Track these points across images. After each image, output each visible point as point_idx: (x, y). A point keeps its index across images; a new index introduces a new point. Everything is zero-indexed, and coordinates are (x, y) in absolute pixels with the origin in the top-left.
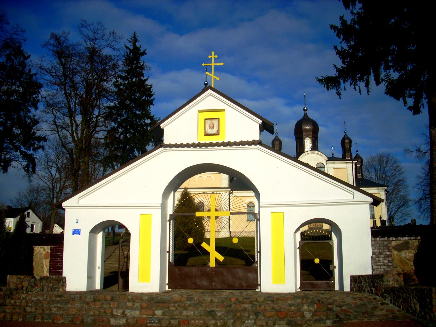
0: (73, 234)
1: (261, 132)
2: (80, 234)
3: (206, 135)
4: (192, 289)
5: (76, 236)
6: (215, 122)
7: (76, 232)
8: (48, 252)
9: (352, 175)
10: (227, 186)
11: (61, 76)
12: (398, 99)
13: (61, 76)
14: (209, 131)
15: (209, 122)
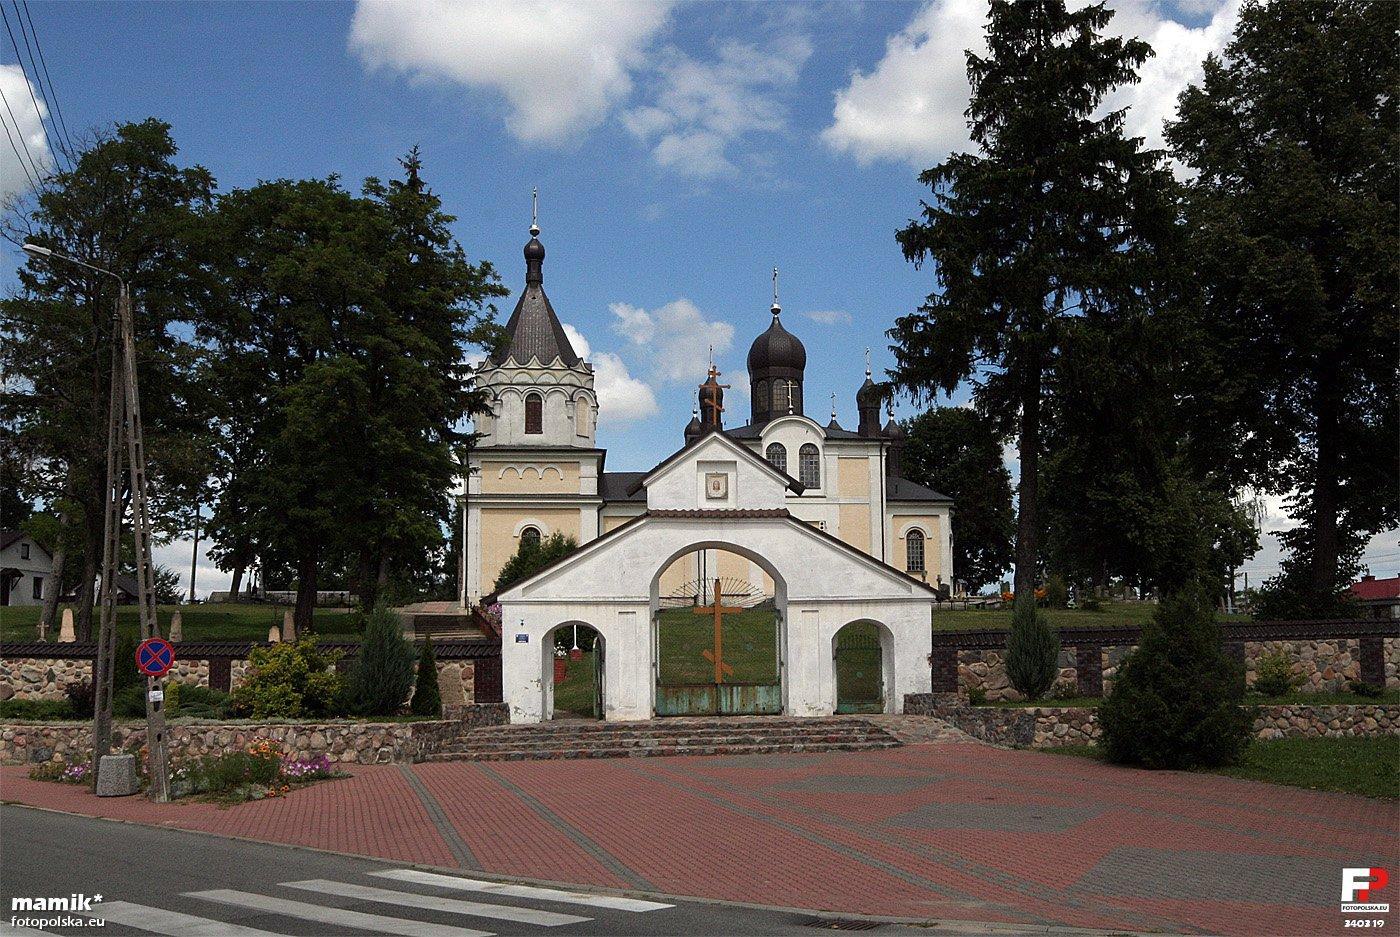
3: (710, 498)
6: (722, 481)
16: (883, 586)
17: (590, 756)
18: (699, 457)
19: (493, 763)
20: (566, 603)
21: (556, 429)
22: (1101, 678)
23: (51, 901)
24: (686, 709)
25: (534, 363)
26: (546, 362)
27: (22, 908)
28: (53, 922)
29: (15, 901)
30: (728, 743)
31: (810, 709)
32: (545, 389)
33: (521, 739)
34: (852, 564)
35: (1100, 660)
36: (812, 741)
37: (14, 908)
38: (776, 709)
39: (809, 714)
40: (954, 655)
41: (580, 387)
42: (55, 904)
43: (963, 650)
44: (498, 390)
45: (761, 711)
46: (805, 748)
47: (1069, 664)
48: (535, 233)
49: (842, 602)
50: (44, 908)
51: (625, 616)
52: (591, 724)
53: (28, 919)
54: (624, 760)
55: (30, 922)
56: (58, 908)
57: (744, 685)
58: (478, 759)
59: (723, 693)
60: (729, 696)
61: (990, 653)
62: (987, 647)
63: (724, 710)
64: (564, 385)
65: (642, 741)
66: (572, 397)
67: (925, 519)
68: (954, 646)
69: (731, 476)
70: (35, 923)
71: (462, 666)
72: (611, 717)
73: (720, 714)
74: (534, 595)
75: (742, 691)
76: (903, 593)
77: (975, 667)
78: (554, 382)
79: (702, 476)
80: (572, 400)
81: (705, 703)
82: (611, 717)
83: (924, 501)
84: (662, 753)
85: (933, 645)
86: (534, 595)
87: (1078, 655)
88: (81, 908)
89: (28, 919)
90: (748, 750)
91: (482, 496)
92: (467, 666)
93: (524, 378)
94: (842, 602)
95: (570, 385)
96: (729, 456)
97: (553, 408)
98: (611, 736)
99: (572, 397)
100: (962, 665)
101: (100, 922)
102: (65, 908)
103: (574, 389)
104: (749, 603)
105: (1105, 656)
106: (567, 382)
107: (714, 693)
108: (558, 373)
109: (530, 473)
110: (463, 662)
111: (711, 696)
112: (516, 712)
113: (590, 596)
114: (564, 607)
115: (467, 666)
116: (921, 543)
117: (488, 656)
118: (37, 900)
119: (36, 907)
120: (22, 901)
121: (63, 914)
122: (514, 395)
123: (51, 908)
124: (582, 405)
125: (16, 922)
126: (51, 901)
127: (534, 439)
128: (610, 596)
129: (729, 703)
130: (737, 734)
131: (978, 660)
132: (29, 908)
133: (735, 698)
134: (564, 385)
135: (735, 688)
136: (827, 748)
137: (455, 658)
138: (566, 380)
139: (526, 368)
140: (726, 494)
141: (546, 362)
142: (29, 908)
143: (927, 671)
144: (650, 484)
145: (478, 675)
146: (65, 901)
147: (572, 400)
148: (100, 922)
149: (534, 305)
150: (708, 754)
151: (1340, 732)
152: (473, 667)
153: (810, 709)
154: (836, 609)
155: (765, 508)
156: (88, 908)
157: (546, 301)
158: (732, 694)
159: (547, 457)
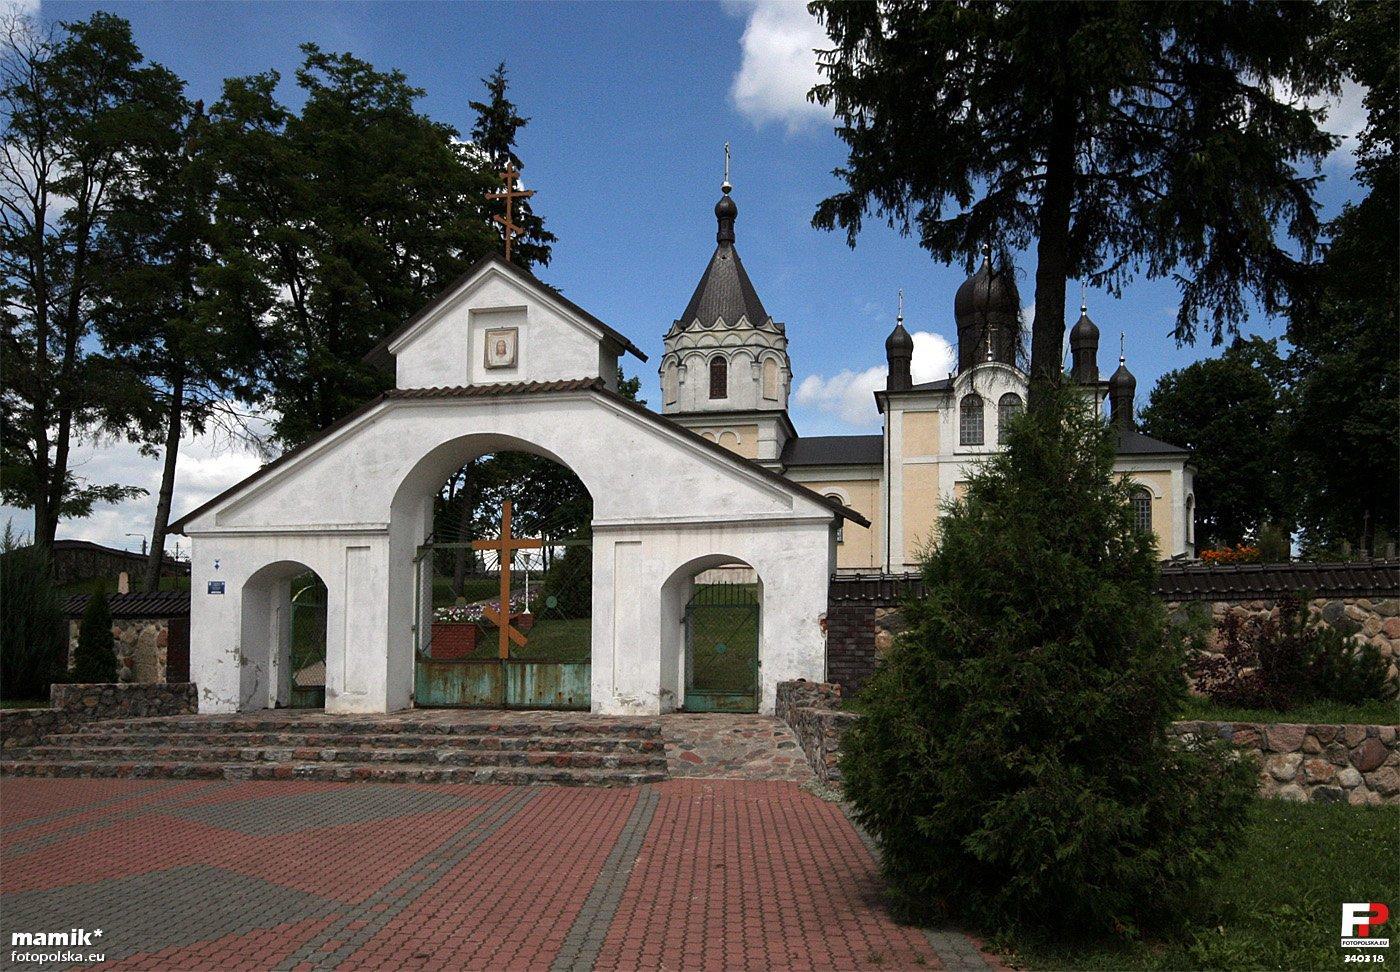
0: (209, 592)
1: (403, 384)
2: (223, 592)
3: (491, 368)
4: (541, 709)
5: (216, 597)
6: (509, 340)
7: (217, 588)
8: (164, 631)
9: (246, 541)
10: (772, 457)
11: (1085, 151)
12: (947, 259)
13: (1085, 151)
14: (496, 360)
15: (495, 339)
16: (749, 498)
18: (476, 302)
19: (37, 779)
20: (276, 534)
21: (742, 392)
23: (51, 936)
24: (456, 696)
25: (720, 325)
26: (731, 323)
27: (22, 943)
28: (53, 957)
29: (15, 936)
30: (396, 760)
31: (623, 702)
32: (730, 351)
33: (126, 740)
34: (696, 462)
36: (527, 763)
37: (14, 943)
39: (621, 711)
41: (767, 348)
42: (55, 939)
44: (682, 354)
45: (566, 702)
46: (494, 776)
48: (727, 190)
49: (678, 527)
50: (44, 943)
51: (357, 553)
53: (28, 954)
54: (216, 783)
55: (30, 958)
56: (58, 943)
57: (542, 662)
58: (20, 772)
63: (511, 700)
64: (750, 345)
66: (757, 358)
67: (1154, 476)
70: (35, 957)
73: (506, 707)
75: (539, 671)
76: (779, 510)
78: (739, 343)
79: (479, 335)
80: (757, 361)
81: (484, 689)
83: (1150, 454)
85: (829, 597)
88: (80, 943)
89: (28, 954)
90: (403, 775)
93: (709, 341)
94: (678, 527)
95: (755, 345)
96: (514, 298)
97: (738, 371)
98: (246, 739)
99: (757, 358)
100: (883, 634)
101: (100, 957)
102: (65, 943)
103: (760, 349)
106: (753, 343)
108: (745, 333)
111: (494, 678)
112: (206, 696)
113: (306, 523)
116: (1148, 504)
118: (37, 935)
119: (36, 942)
120: (22, 936)
121: (64, 949)
122: (698, 360)
123: (51, 943)
124: (769, 366)
125: (16, 957)
126: (51, 936)
127: (719, 404)
128: (333, 522)
129: (519, 690)
132: (29, 943)
133: (528, 679)
134: (750, 345)
135: (528, 667)
136: (531, 778)
138: (751, 341)
139: (711, 331)
141: (731, 323)
142: (29, 943)
144: (401, 349)
146: (65, 936)
147: (757, 361)
148: (100, 957)
149: (725, 265)
150: (342, 780)
153: (623, 702)
154: (669, 539)
155: (567, 377)
156: (88, 943)
157: (737, 259)
158: (523, 677)
159: (728, 420)
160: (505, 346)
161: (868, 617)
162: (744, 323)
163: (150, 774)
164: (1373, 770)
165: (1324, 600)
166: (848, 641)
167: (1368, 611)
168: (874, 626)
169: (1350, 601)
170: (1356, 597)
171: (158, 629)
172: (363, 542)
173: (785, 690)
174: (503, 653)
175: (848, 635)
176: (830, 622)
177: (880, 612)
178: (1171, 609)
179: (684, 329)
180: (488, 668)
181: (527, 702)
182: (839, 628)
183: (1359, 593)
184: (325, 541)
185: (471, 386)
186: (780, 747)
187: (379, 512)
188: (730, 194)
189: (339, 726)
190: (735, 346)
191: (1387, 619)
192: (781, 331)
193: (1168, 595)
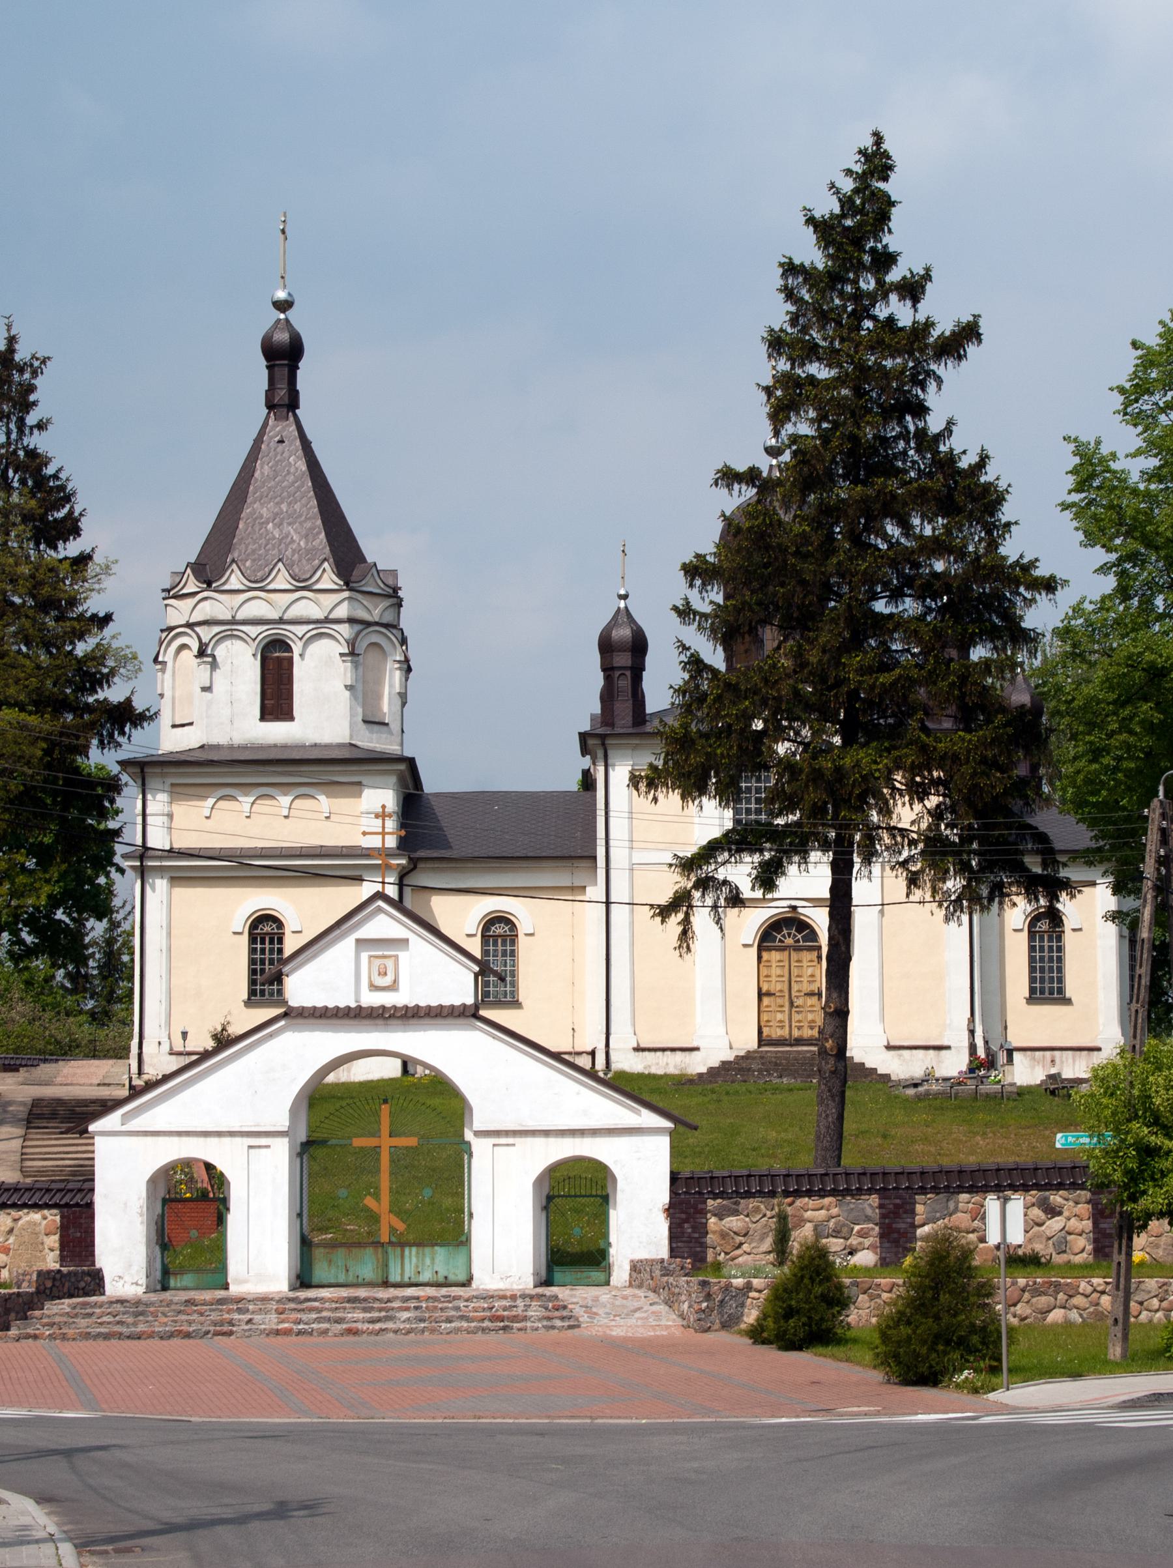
3: (374, 988)
15: (378, 962)
17: (188, 1335)
20: (179, 1134)
22: (914, 1239)
32: (300, 630)
35: (913, 1212)
38: (462, 1277)
40: (700, 1206)
43: (714, 1199)
47: (868, 1219)
49: (546, 1133)
52: (221, 1294)
59: (391, 1257)
60: (1124, 1242)
61: (752, 1203)
62: (748, 1195)
65: (257, 1318)
68: (700, 1193)
69: (403, 956)
71: (45, 1218)
72: (235, 1289)
73: (386, 1284)
74: (136, 1124)
75: (418, 1253)
77: (734, 1222)
79: (364, 956)
82: (235, 1289)
84: (278, 1332)
86: (136, 1124)
87: (881, 1206)
91: (172, 853)
92: (50, 1218)
93: (258, 608)
94: (546, 1133)
104: (697, 1065)
105: (919, 1208)
107: (380, 1256)
109: (264, 806)
110: (46, 1212)
114: (176, 1139)
115: (50, 1218)
117: (77, 1205)
127: (277, 732)
129: (399, 1271)
130: (380, 1310)
131: (736, 1213)
137: (36, 1206)
140: (395, 981)
143: (662, 1227)
145: (63, 1229)
151: (1160, 1314)
152: (58, 1218)
154: (540, 1141)
155: (446, 1002)
160: (386, 968)
161: (700, 1206)
162: (328, 579)
163: (171, 1335)
164: (1015, 1305)
165: (1036, 1192)
166: (686, 1225)
167: (1067, 1200)
168: (706, 1214)
169: (1055, 1192)
170: (1058, 1190)
171: (45, 1218)
172: (263, 1141)
173: (636, 1267)
174: (385, 1238)
175: (686, 1221)
176: (671, 1211)
177: (710, 1202)
178: (929, 1199)
179: (209, 584)
180: (369, 1251)
181: (406, 1280)
182: (677, 1215)
183: (1060, 1186)
184: (226, 1140)
185: (360, 1007)
186: (651, 1304)
187: (282, 1121)
188: (292, 314)
189: (239, 1300)
190: (308, 622)
191: (1080, 1206)
192: (393, 596)
193: (926, 1189)
